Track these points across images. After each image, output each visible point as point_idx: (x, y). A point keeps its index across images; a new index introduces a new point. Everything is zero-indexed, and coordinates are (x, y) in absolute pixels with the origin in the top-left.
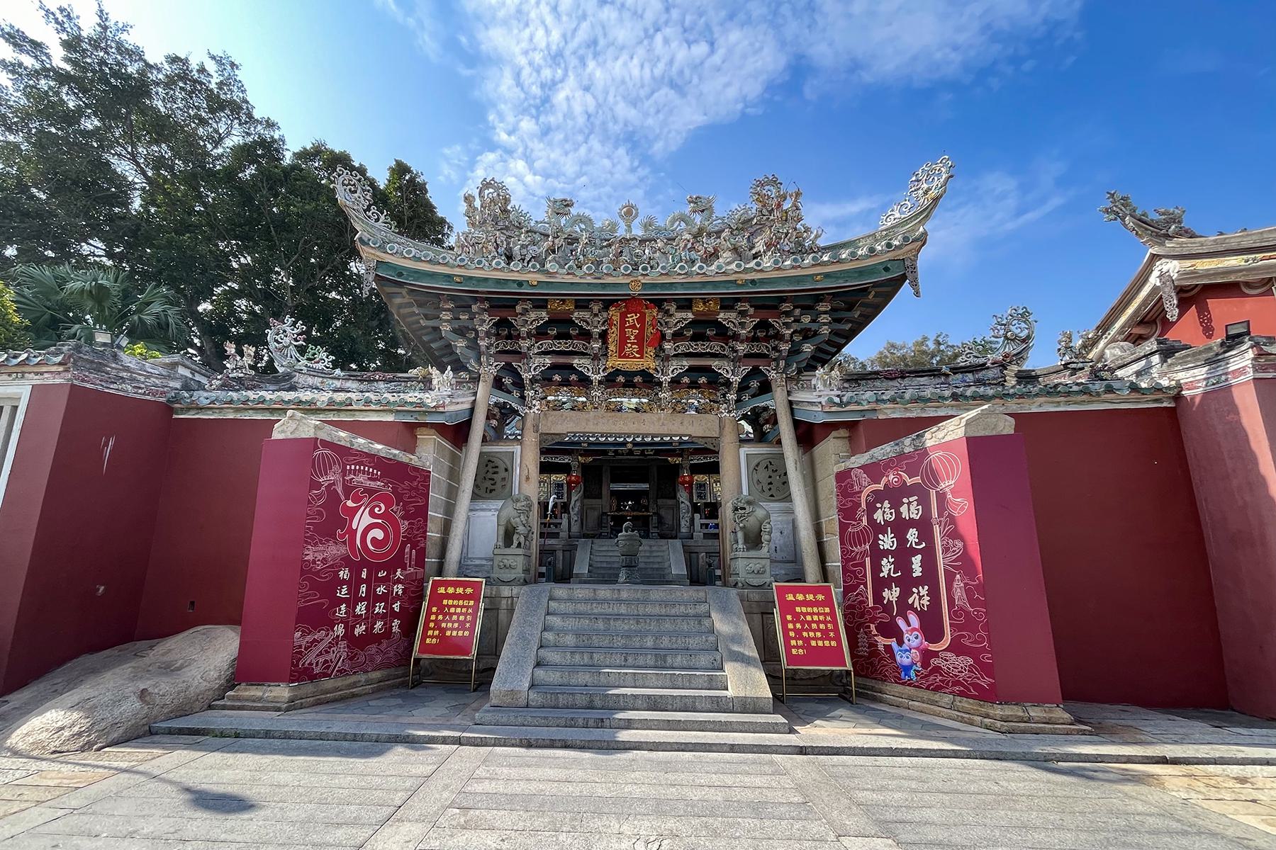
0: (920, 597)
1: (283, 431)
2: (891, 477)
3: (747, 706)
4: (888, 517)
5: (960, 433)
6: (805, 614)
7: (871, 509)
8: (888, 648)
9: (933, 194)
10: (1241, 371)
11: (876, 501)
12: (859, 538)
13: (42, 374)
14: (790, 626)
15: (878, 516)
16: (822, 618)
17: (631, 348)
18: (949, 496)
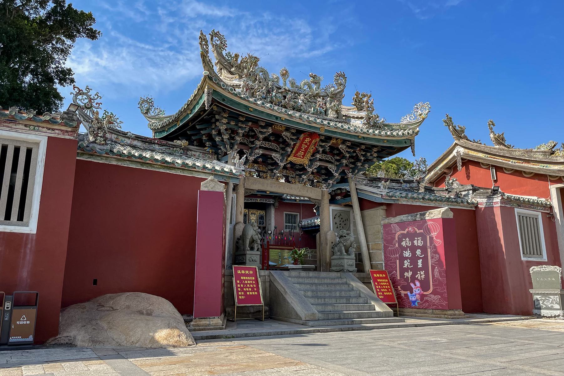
0: (421, 275)
1: (206, 187)
2: (410, 229)
3: (386, 315)
4: (408, 244)
5: (440, 216)
6: (245, 280)
7: (400, 241)
8: (406, 295)
9: (423, 116)
10: (497, 203)
11: (403, 238)
12: (394, 252)
13: (53, 130)
14: (239, 286)
15: (403, 244)
16: (251, 282)
17: (301, 153)
18: (434, 238)
